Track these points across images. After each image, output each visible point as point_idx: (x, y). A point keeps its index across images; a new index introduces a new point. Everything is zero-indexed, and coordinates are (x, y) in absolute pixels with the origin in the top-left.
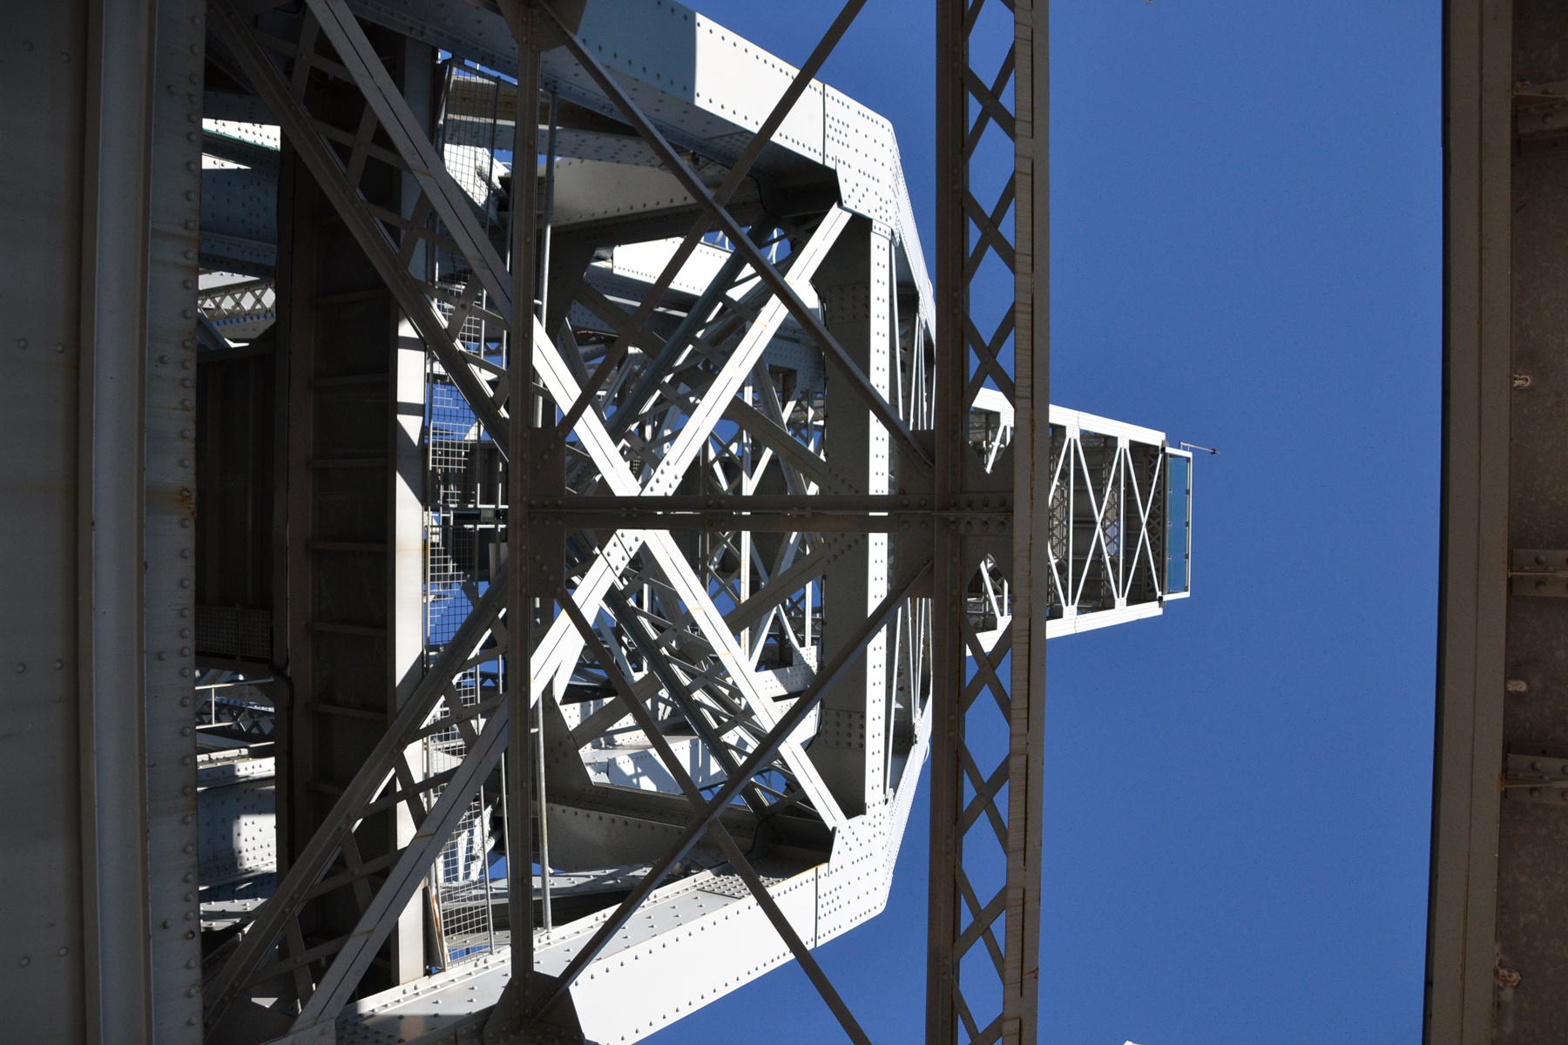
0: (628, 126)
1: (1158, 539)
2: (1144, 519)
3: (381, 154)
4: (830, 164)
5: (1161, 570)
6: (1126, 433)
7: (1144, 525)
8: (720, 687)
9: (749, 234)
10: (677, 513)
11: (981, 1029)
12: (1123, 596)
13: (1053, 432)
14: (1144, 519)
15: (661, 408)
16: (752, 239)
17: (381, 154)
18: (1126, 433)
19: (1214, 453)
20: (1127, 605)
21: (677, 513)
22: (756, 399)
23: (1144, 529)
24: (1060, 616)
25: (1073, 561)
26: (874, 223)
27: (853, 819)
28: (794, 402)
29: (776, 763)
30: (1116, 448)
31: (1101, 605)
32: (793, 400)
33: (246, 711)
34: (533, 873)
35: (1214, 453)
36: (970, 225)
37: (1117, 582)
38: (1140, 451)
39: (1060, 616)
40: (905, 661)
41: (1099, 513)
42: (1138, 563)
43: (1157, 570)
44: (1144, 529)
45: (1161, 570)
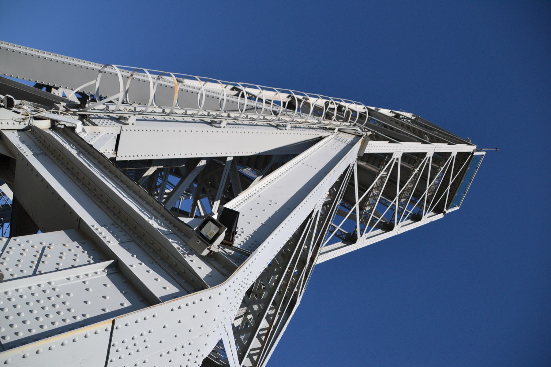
0: (70, 108)
1: (455, 188)
2: (451, 183)
5: (450, 200)
6: (455, 149)
7: (450, 185)
9: (295, 291)
14: (451, 183)
15: (460, 174)
16: (295, 292)
18: (455, 149)
19: (497, 150)
22: (322, 213)
28: (219, 201)
30: (450, 156)
32: (218, 200)
33: (356, 123)
34: (202, 200)
35: (497, 150)
38: (462, 156)
40: (296, 259)
41: (429, 185)
42: (440, 201)
43: (448, 199)
44: (449, 187)
45: (450, 200)
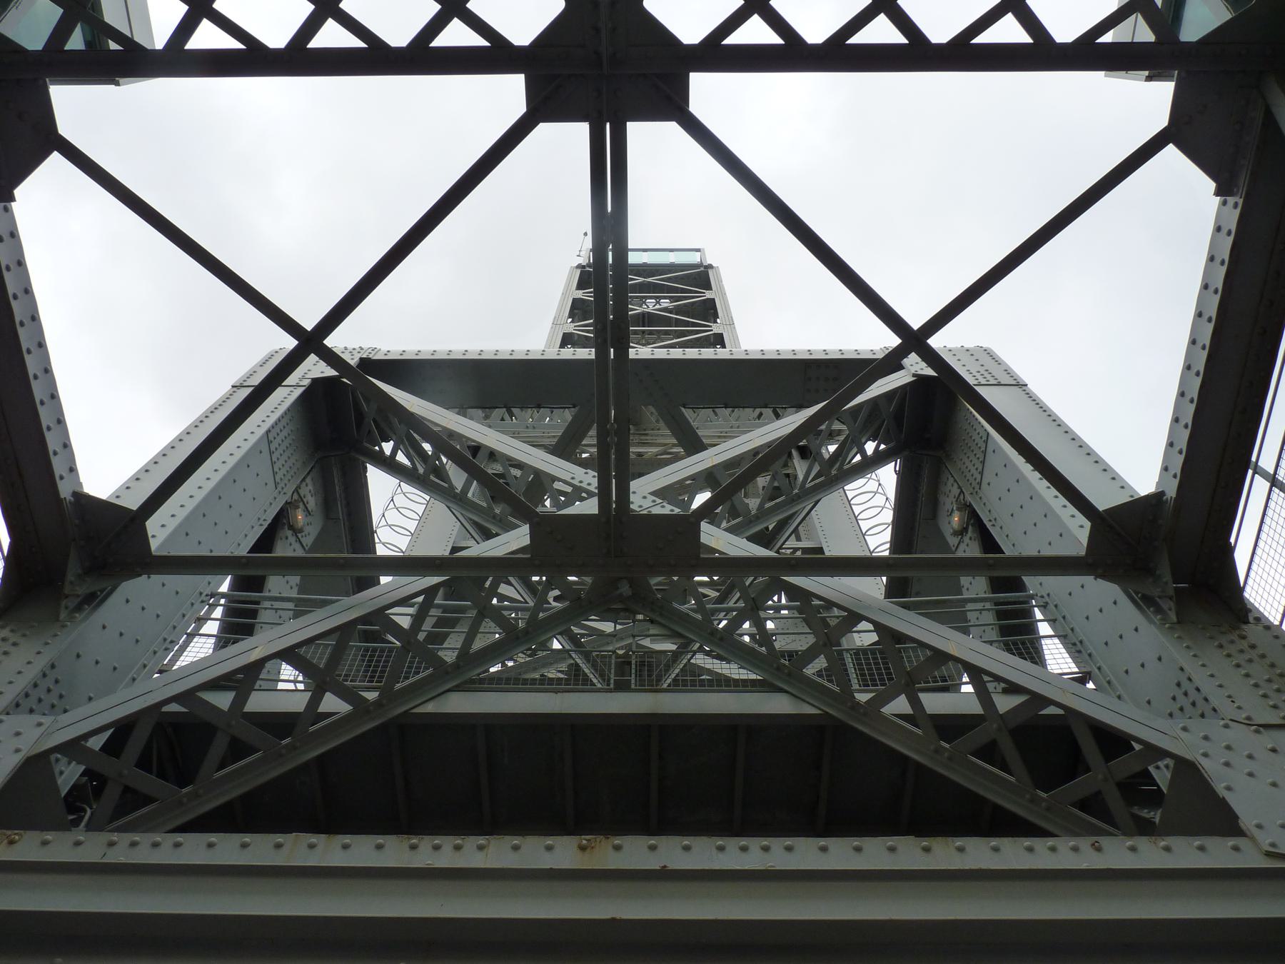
2: (641, 280)
3: (134, 747)
4: (306, 382)
8: (753, 677)
10: (610, 253)
11: (873, 629)
12: (704, 293)
13: (578, 309)
17: (134, 747)
20: (712, 290)
21: (610, 253)
23: (650, 280)
24: (721, 335)
25: (676, 327)
26: (364, 356)
27: (1108, 78)
29: (816, 602)
31: (712, 311)
36: (240, 44)
37: (693, 297)
39: (721, 335)
44: (650, 280)
